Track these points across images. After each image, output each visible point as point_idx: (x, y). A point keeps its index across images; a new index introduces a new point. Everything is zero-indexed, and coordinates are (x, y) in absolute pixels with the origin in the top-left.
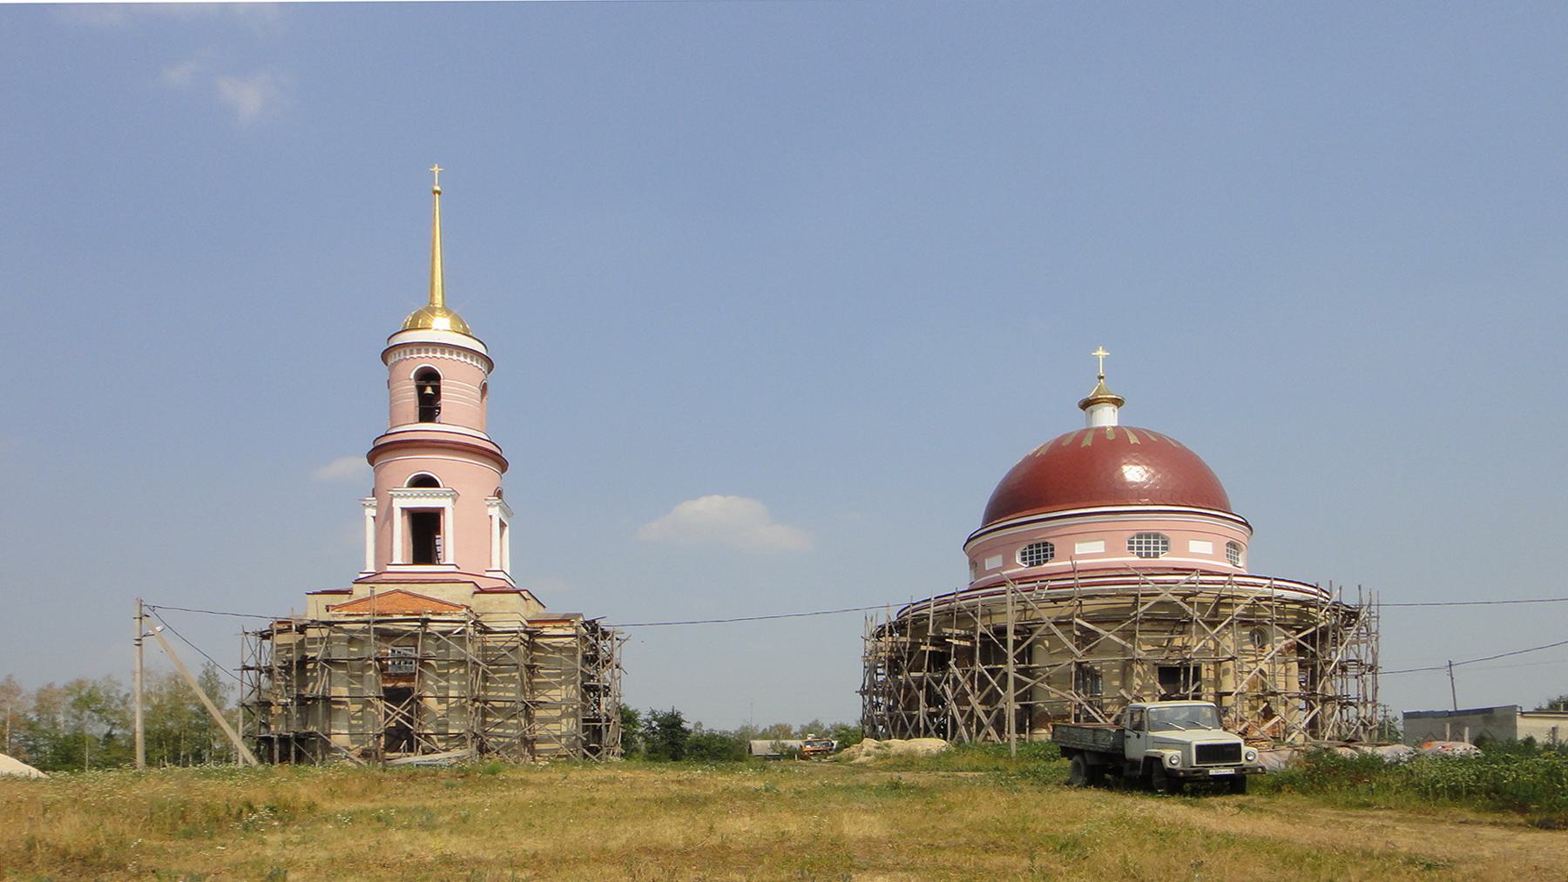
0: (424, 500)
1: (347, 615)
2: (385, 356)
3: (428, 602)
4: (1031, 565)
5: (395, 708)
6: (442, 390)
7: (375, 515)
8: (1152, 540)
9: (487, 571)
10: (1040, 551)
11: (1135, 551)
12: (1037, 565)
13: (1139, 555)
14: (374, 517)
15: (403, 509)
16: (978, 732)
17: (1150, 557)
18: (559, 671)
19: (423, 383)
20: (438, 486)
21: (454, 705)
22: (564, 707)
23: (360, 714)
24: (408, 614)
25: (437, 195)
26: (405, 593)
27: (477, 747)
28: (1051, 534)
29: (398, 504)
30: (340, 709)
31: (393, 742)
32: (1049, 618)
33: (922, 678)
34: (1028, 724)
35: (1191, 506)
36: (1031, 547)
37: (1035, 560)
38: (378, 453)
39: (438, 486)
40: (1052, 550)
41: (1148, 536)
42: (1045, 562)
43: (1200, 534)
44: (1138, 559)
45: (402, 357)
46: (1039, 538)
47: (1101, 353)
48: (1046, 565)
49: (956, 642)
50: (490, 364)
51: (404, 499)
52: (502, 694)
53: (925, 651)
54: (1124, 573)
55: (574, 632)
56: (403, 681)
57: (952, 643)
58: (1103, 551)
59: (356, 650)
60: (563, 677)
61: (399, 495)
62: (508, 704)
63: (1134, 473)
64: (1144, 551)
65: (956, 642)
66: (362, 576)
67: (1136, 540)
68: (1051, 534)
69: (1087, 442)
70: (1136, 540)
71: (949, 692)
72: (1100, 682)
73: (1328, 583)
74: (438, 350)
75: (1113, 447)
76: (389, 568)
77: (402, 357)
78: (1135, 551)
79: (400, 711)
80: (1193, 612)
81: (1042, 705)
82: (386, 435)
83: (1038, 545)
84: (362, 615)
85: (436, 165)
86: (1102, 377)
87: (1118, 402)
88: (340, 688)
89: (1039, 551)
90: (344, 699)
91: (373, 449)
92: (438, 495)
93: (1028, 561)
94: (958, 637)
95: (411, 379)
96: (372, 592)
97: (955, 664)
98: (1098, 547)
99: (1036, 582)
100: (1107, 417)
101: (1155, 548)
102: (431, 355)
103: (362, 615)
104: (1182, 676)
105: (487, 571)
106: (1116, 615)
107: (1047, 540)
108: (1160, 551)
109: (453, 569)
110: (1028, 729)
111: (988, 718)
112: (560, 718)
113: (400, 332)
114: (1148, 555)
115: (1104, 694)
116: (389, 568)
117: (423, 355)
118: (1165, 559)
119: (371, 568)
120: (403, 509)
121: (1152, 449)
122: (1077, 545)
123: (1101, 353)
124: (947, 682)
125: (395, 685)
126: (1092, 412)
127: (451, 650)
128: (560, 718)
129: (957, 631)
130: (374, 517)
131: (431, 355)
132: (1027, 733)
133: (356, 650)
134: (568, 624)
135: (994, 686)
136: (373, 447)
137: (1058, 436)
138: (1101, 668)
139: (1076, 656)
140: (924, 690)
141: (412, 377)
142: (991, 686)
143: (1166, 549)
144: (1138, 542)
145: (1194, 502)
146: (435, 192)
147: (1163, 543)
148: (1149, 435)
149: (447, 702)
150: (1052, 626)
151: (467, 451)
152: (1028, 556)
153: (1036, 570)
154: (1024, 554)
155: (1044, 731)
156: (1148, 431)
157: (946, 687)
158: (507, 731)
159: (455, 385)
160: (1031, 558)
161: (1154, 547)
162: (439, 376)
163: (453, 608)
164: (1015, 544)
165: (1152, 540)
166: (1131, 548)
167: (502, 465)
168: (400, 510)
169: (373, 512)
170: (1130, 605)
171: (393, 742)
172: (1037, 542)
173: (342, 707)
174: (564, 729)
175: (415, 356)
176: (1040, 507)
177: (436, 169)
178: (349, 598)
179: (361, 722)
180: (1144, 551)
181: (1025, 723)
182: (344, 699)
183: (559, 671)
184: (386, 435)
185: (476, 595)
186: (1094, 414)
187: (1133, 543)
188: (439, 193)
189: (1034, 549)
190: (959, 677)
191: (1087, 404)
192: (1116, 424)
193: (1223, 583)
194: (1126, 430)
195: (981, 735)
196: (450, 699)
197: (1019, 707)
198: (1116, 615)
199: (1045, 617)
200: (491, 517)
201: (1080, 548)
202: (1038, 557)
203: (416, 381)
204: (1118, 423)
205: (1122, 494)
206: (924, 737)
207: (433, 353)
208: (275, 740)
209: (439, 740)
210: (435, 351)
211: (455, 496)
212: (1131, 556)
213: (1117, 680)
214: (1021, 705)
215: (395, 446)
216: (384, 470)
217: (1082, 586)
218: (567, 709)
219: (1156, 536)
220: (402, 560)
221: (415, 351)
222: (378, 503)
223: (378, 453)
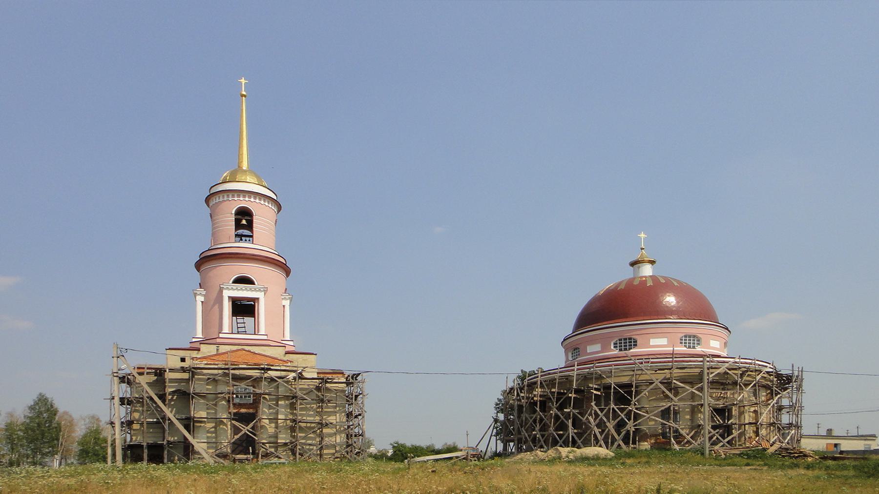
0: (243, 292)
1: (206, 364)
2: (207, 200)
3: (263, 358)
4: (621, 350)
5: (245, 427)
6: (254, 222)
7: (203, 300)
8: (688, 339)
9: (282, 340)
10: (695, 339)
11: (683, 344)
12: (693, 348)
13: (685, 346)
14: (202, 302)
15: (229, 297)
16: (612, 443)
17: (690, 348)
18: (335, 405)
19: (239, 217)
20: (254, 284)
21: (282, 425)
22: (338, 427)
23: (213, 429)
24: (250, 365)
25: (244, 98)
26: (247, 351)
27: (825, 460)
28: (634, 333)
29: (226, 294)
30: (201, 426)
31: (237, 447)
32: (657, 380)
33: (570, 412)
34: (637, 439)
35: (711, 321)
36: (620, 340)
37: (623, 348)
38: (205, 260)
39: (254, 284)
40: (636, 342)
41: (690, 337)
42: (630, 349)
43: (716, 337)
44: (685, 349)
45: (221, 200)
46: (627, 335)
47: (642, 235)
48: (631, 350)
49: (595, 392)
50: (279, 208)
51: (231, 291)
52: (305, 418)
53: (571, 397)
54: (650, 357)
55: (345, 380)
56: (244, 409)
57: (593, 392)
58: (666, 344)
59: (211, 387)
60: (338, 409)
61: (232, 288)
62: (309, 425)
63: (670, 300)
64: (687, 345)
65: (595, 392)
66: (194, 340)
67: (684, 338)
68: (634, 333)
69: (636, 282)
70: (684, 338)
71: (592, 420)
72: (678, 416)
73: (791, 365)
74: (247, 196)
75: (661, 286)
76: (221, 335)
77: (226, 199)
78: (683, 344)
79: (245, 429)
80: (738, 378)
81: (645, 429)
82: (209, 250)
83: (625, 339)
84: (217, 364)
85: (243, 78)
86: (643, 249)
87: (652, 262)
88: (201, 412)
89: (690, 340)
90: (203, 420)
91: (199, 260)
92: (255, 290)
93: (618, 348)
94: (596, 389)
95: (232, 214)
96: (217, 350)
97: (595, 404)
98: (663, 341)
99: (643, 359)
100: (647, 270)
101: (694, 343)
102: (247, 199)
103: (217, 364)
104: (727, 413)
105: (282, 340)
106: (690, 379)
107: (632, 337)
108: (696, 345)
109: (265, 337)
110: (637, 442)
111: (619, 436)
112: (335, 434)
113: (221, 183)
114: (690, 347)
115: (681, 422)
116: (221, 335)
117: (241, 199)
118: (699, 350)
119: (199, 334)
120: (229, 297)
121: (683, 291)
122: (651, 340)
123: (642, 235)
124: (590, 415)
125: (238, 411)
126: (639, 267)
127: (280, 389)
128: (335, 434)
129: (595, 386)
130: (202, 302)
131: (247, 199)
132: (637, 444)
133: (211, 387)
134: (341, 375)
135: (622, 418)
136: (199, 259)
137: (620, 281)
138: (679, 408)
139: (674, 401)
140: (571, 419)
141: (233, 212)
142: (620, 418)
143: (699, 344)
144: (620, 343)
145: (701, 317)
146: (243, 96)
147: (634, 342)
148: (673, 282)
149: (277, 422)
150: (660, 385)
151: (276, 265)
152: (618, 345)
153: (623, 353)
154: (615, 344)
155: (646, 443)
156: (671, 278)
157: (590, 418)
158: (308, 442)
159: (264, 221)
160: (685, 343)
161: (627, 343)
162: (253, 214)
163: (281, 362)
164: (612, 338)
165: (688, 339)
166: (681, 343)
167: (287, 271)
168: (227, 298)
169: (202, 299)
170: (697, 374)
171: (237, 447)
172: (620, 338)
173: (202, 425)
174: (338, 440)
175: (236, 199)
176: (620, 319)
177: (243, 81)
178: (198, 354)
179: (214, 435)
180: (687, 345)
181: (636, 439)
182: (203, 420)
183: (335, 405)
184: (209, 250)
185: (287, 355)
186: (640, 269)
187: (617, 344)
188: (245, 96)
189: (623, 341)
190: (599, 412)
191: (633, 264)
192: (651, 275)
193: (751, 364)
194: (658, 277)
195: (614, 446)
196: (279, 420)
197: (634, 430)
198: (690, 379)
199: (655, 380)
200: (284, 306)
201: (653, 342)
202: (694, 343)
203: (235, 215)
204: (653, 273)
205: (661, 312)
206: (595, 446)
207: (249, 198)
208: (145, 446)
209: (270, 447)
210: (239, 196)
211: (265, 291)
212: (681, 347)
213: (688, 415)
214: (635, 429)
215: (224, 256)
216: (214, 270)
217: (741, 363)
218: (340, 428)
219: (694, 336)
220: (229, 330)
221: (230, 196)
222: (206, 293)
223: (205, 260)
